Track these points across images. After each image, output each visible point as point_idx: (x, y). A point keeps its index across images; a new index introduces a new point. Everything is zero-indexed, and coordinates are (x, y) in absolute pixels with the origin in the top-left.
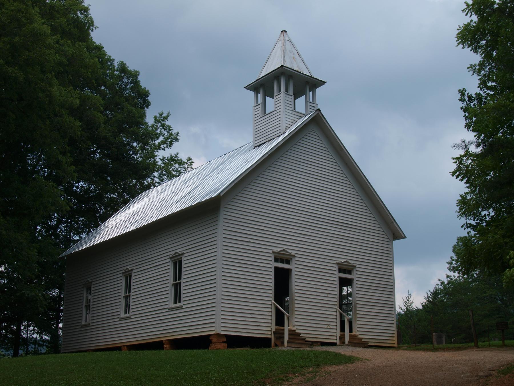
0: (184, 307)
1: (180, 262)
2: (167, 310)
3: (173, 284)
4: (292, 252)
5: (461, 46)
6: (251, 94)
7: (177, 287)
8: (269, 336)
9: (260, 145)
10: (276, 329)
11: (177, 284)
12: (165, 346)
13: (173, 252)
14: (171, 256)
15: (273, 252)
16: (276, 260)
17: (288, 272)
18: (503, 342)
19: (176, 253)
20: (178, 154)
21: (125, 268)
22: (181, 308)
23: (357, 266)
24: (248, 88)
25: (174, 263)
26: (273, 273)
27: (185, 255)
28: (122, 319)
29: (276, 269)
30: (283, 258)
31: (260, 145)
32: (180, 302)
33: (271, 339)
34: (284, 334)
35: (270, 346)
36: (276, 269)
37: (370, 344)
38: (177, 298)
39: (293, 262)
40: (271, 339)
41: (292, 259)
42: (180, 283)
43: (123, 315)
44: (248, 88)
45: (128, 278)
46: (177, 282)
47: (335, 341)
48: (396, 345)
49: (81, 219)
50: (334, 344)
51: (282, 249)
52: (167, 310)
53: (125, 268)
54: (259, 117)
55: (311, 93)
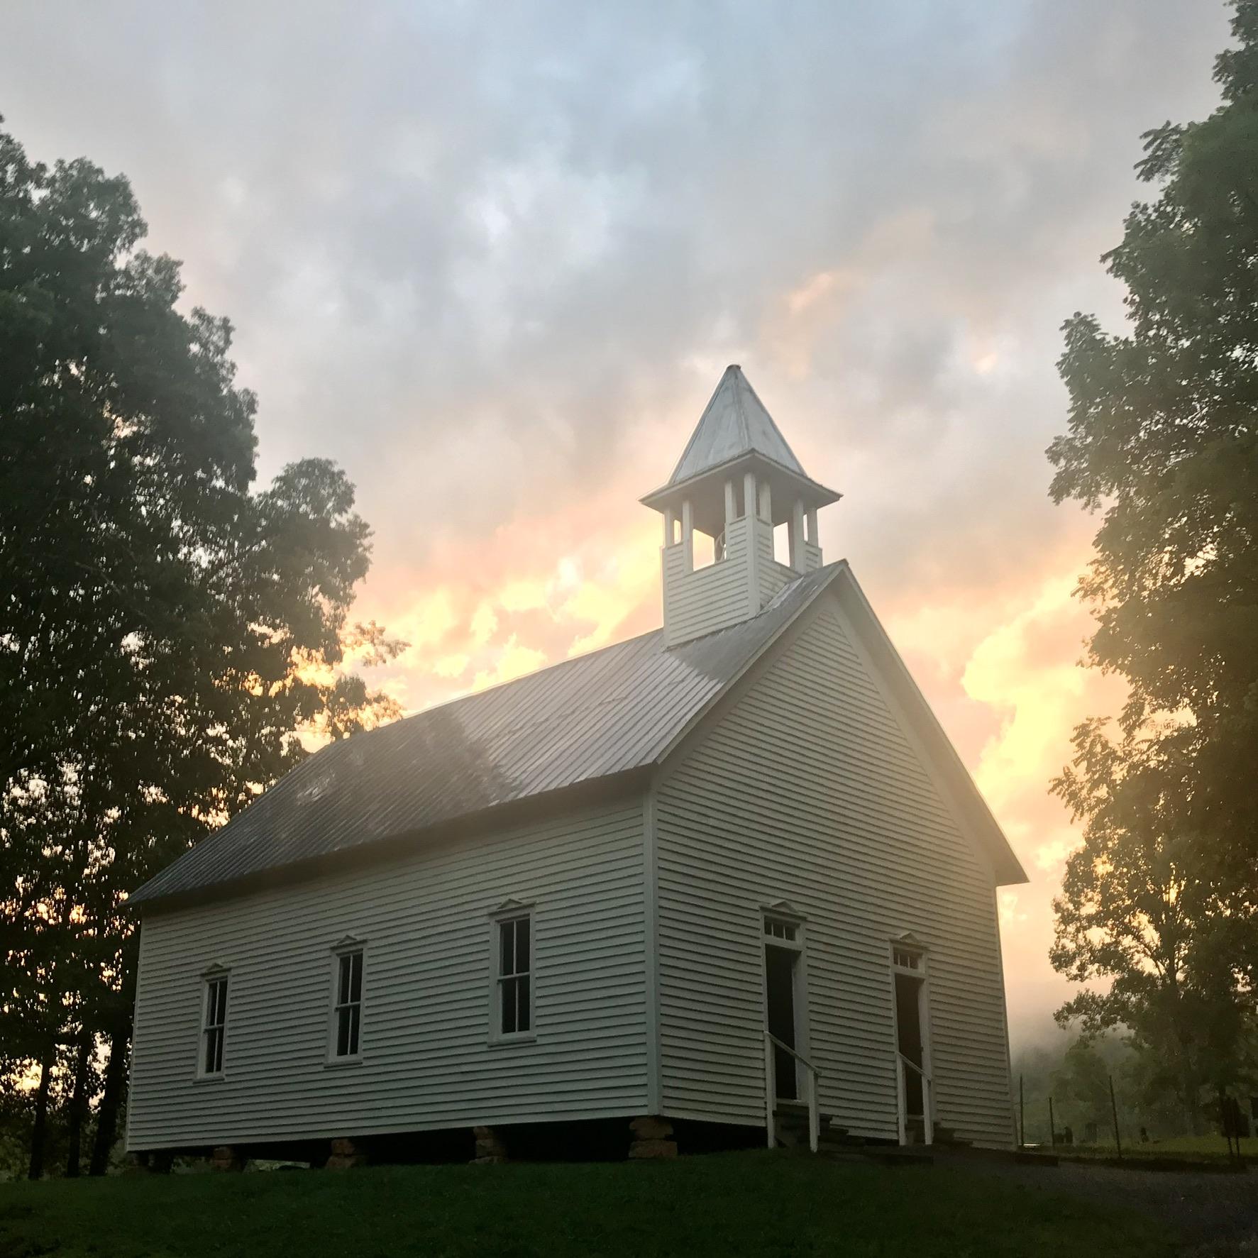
0: (540, 1041)
1: (224, 985)
2: (484, 1048)
3: (206, 1031)
4: (800, 909)
6: (656, 518)
7: (215, 1038)
8: (761, 1124)
10: (778, 1105)
11: (348, 1009)
12: (479, 1142)
15: (763, 909)
17: (791, 957)
19: (217, 965)
22: (220, 1081)
25: (342, 960)
26: (762, 961)
27: (539, 909)
28: (329, 1068)
29: (770, 949)
30: (781, 923)
32: (219, 1069)
33: (764, 1130)
34: (808, 1118)
36: (770, 949)
38: (348, 1041)
40: (764, 1130)
41: (798, 925)
42: (221, 1030)
43: (201, 1074)
46: (349, 1003)
51: (780, 901)
52: (484, 1048)
54: (681, 575)
55: (805, 517)
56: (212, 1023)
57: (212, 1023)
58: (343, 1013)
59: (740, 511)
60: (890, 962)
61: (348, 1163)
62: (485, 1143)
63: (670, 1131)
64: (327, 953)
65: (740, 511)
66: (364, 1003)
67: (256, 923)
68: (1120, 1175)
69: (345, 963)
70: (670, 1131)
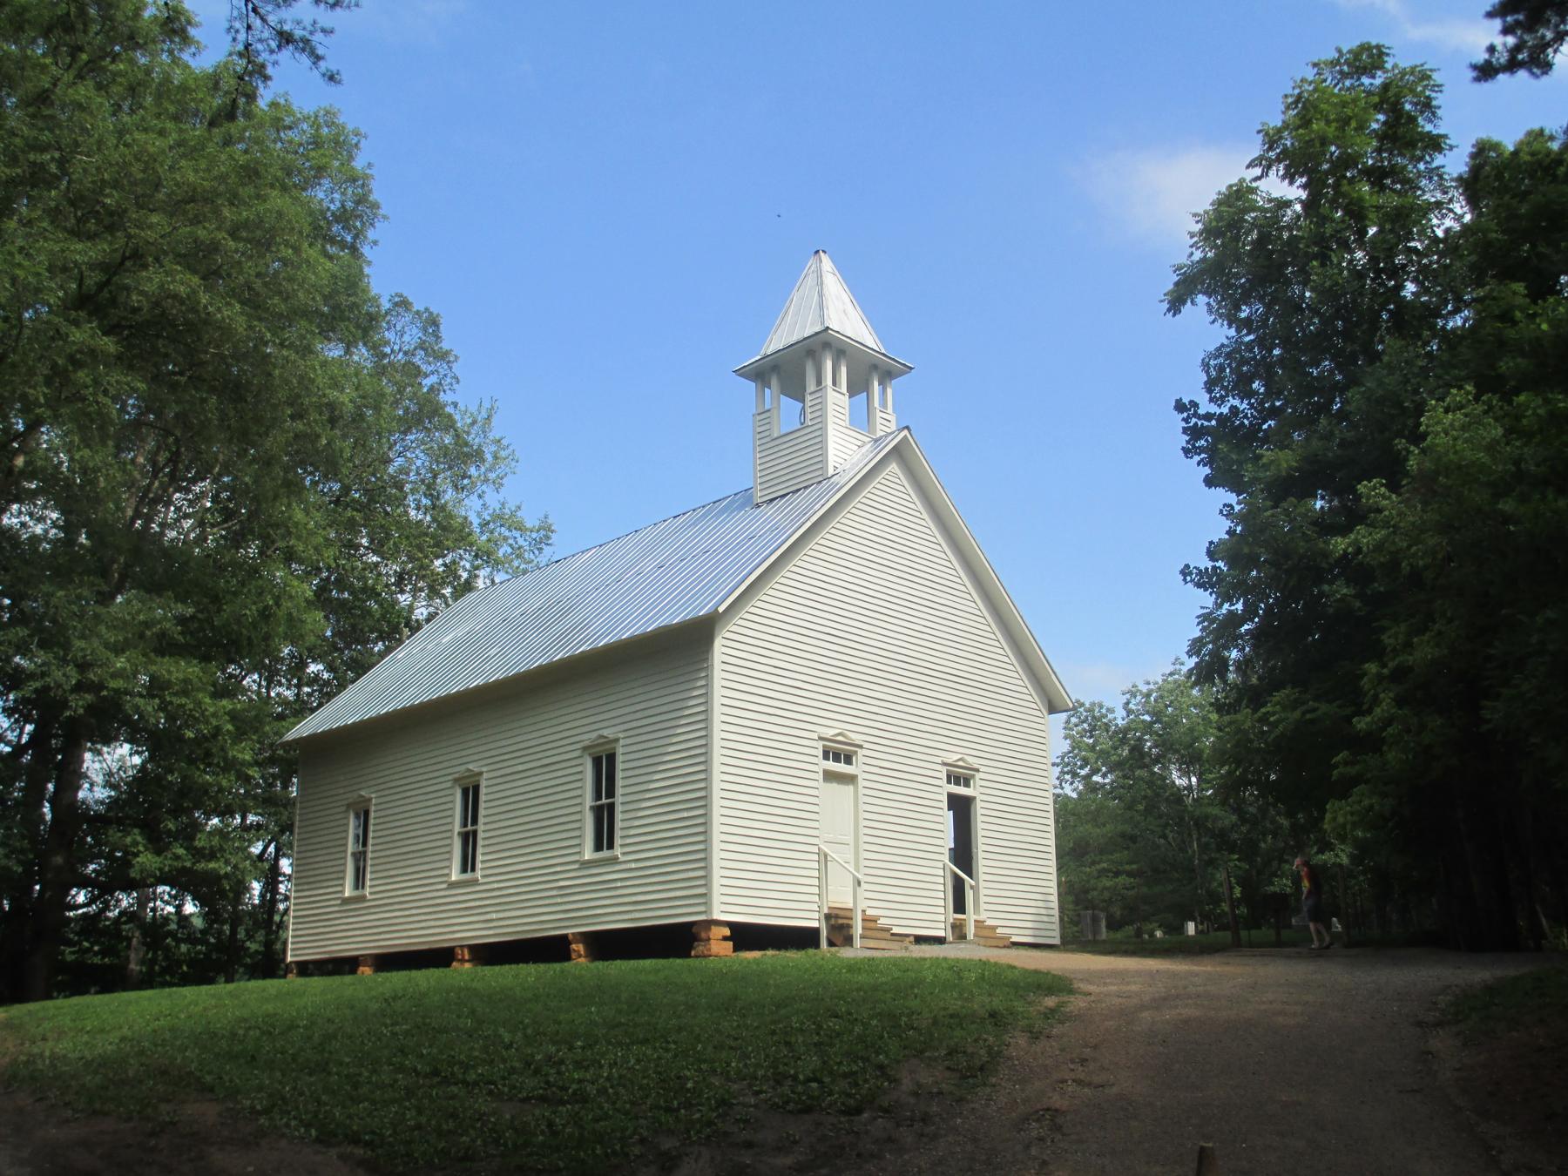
4: (857, 738)
5: (1166, 305)
8: (815, 924)
9: (772, 500)
12: (574, 946)
13: (594, 735)
14: (587, 743)
16: (826, 756)
18: (1278, 934)
19: (602, 737)
20: (1486, 71)
21: (463, 768)
23: (982, 769)
24: (742, 373)
28: (452, 885)
31: (772, 500)
35: (817, 945)
37: (1015, 939)
38: (604, 838)
39: (860, 757)
43: (455, 876)
44: (742, 373)
45: (471, 795)
46: (604, 801)
47: (941, 933)
48: (1057, 941)
49: (1308, 294)
50: (940, 941)
53: (463, 768)
56: (465, 825)
57: (465, 825)
58: (598, 811)
59: (884, 404)
60: (861, 776)
61: (467, 965)
62: (578, 947)
63: (727, 932)
64: (577, 754)
65: (884, 404)
66: (481, 827)
67: (504, 743)
68: (397, 979)
69: (597, 762)
70: (727, 932)
